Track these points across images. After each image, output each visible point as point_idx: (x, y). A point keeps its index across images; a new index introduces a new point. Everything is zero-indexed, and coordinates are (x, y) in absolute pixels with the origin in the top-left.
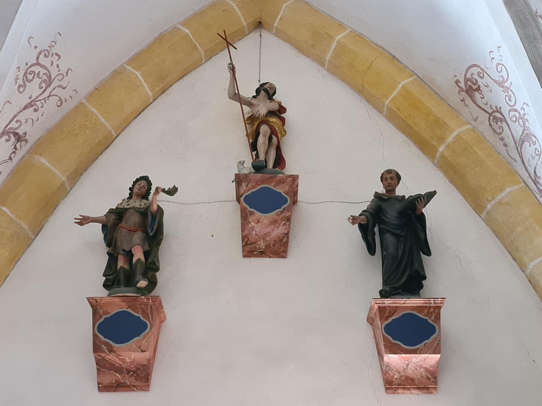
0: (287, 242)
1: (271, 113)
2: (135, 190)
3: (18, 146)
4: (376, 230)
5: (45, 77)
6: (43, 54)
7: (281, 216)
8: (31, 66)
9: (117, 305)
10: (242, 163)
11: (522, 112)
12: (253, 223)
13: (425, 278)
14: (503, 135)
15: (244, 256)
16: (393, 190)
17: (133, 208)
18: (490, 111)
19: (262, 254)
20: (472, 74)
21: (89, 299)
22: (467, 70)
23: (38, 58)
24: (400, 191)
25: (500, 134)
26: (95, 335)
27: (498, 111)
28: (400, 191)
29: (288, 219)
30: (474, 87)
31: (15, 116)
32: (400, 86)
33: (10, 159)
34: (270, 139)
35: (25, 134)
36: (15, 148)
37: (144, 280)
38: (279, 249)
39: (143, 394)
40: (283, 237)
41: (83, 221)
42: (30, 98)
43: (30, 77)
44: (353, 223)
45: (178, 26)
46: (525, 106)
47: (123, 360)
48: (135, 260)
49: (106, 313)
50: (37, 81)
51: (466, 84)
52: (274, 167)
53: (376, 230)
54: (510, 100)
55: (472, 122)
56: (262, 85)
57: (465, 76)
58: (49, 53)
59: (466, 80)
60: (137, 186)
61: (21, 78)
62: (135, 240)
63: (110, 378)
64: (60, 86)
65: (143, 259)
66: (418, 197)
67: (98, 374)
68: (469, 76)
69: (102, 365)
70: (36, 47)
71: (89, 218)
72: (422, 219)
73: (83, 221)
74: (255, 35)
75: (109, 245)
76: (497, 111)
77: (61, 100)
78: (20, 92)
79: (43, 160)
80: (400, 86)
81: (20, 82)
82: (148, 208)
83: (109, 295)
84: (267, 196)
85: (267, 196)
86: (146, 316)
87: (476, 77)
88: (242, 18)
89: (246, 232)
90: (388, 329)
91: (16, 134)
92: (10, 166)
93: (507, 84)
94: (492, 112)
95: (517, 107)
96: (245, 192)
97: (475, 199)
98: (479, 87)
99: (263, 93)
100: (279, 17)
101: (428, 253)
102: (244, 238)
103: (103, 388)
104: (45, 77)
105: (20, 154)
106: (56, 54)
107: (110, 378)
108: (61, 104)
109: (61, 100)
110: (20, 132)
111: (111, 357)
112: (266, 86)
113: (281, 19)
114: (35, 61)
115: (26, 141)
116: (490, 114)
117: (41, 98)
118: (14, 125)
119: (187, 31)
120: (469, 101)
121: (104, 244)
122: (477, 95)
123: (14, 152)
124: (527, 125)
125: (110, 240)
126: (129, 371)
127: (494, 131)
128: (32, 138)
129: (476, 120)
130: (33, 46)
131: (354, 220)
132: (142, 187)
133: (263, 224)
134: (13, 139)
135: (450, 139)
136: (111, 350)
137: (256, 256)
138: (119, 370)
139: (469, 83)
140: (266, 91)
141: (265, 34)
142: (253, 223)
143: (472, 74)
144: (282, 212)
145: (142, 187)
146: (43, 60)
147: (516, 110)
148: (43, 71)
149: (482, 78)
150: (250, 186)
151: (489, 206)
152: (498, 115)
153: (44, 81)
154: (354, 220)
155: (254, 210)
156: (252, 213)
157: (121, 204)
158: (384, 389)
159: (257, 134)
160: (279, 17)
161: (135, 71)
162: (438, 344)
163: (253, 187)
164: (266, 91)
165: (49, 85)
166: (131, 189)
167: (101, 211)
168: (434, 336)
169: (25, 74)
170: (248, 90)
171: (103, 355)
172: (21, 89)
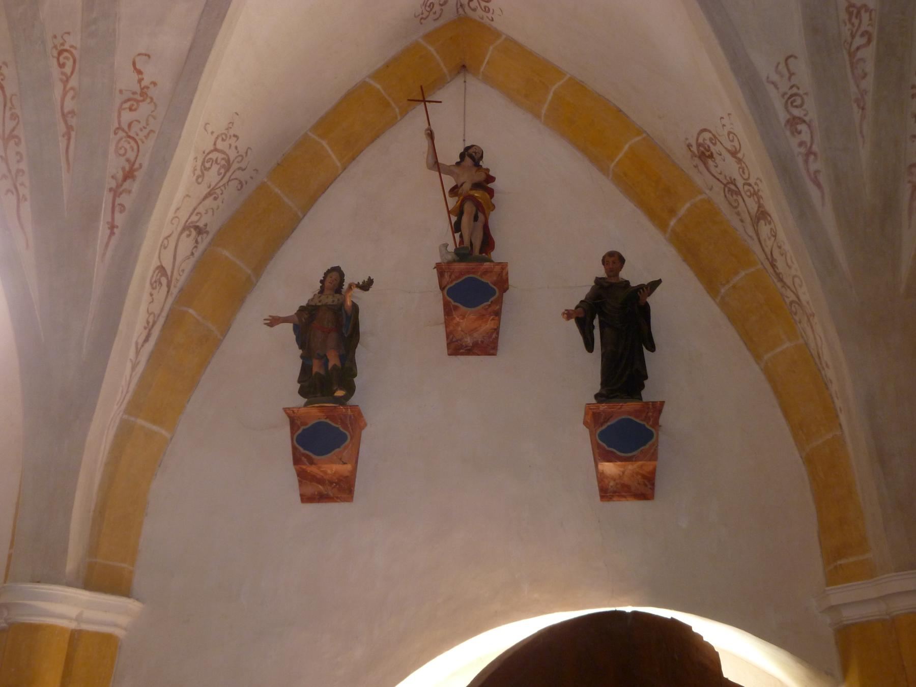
0: (497, 338)
1: (477, 186)
2: (327, 284)
3: (199, 239)
4: (596, 322)
5: (223, 162)
6: (220, 139)
7: (490, 310)
8: (208, 154)
9: (315, 414)
10: (446, 246)
11: (756, 187)
12: (458, 319)
13: (646, 377)
14: (739, 209)
15: (449, 355)
16: (617, 275)
17: (326, 305)
18: (725, 182)
19: (469, 351)
20: (704, 139)
21: (285, 410)
22: (699, 134)
23: (215, 144)
24: (624, 274)
25: (736, 207)
26: (294, 449)
27: (733, 182)
28: (624, 274)
29: (498, 314)
30: (708, 154)
31: (195, 209)
32: (626, 147)
33: (192, 254)
34: (476, 218)
35: (206, 225)
36: (197, 242)
37: (341, 389)
38: (487, 346)
39: (345, 505)
40: (492, 333)
41: (273, 321)
42: (209, 187)
43: (208, 165)
44: (568, 318)
45: (367, 80)
46: (758, 182)
47: (325, 473)
48: (330, 365)
49: (303, 424)
50: (215, 168)
51: (698, 150)
52: (481, 252)
53: (596, 322)
54: (744, 173)
55: (707, 191)
56: (467, 149)
57: (697, 140)
58: (226, 135)
59: (699, 145)
60: (328, 279)
61: (198, 168)
62: (329, 333)
63: (311, 489)
64: (239, 169)
65: (338, 363)
66: (641, 287)
67: (300, 486)
68: (701, 141)
69: (303, 477)
70: (212, 133)
71: (280, 318)
72: (645, 310)
73: (273, 321)
74: (458, 82)
75: (301, 347)
76: (732, 183)
77: (241, 183)
78: (199, 183)
79: (226, 253)
80: (626, 147)
81: (198, 172)
82: (342, 305)
83: (306, 405)
84: (473, 287)
85: (473, 287)
86: (345, 427)
87: (708, 142)
88: (442, 64)
89: (451, 328)
90: (602, 435)
91: (196, 228)
92: (193, 260)
93: (740, 155)
94: (728, 183)
95: (752, 181)
96: (448, 283)
97: (710, 279)
98: (712, 154)
99: (468, 161)
100: (486, 60)
101: (652, 348)
102: (448, 335)
103: (306, 499)
104: (223, 162)
105: (201, 247)
106: (235, 136)
107: (311, 489)
108: (242, 186)
109: (241, 183)
110: (201, 224)
111: (312, 469)
112: (470, 151)
113: (488, 63)
114: (212, 148)
115: (207, 233)
116: (725, 185)
117: (221, 184)
118: (194, 218)
119: (379, 86)
120: (702, 167)
121: (295, 346)
122: (710, 163)
123: (196, 247)
124: (762, 202)
125: (303, 341)
126: (331, 483)
127: (731, 204)
128: (213, 229)
129: (711, 189)
130: (209, 131)
131: (568, 315)
132: (334, 279)
133: (469, 321)
134: (194, 233)
135: (683, 210)
136: (312, 462)
137: (462, 354)
138: (321, 481)
139: (702, 149)
140: (471, 156)
141: (471, 79)
142: (458, 319)
143: (704, 139)
144: (490, 306)
145: (334, 279)
146: (220, 145)
147: (750, 185)
148: (220, 156)
149: (715, 144)
150: (453, 277)
151: (723, 291)
152: (733, 187)
153: (223, 167)
154: (568, 315)
155: (459, 305)
156: (456, 308)
157: (312, 300)
158: (599, 498)
159: (460, 213)
160: (486, 60)
161: (320, 140)
162: (656, 450)
163: (457, 278)
164: (471, 156)
165: (227, 170)
166: (322, 282)
167: (291, 310)
168: (650, 443)
169: (203, 164)
170: (450, 154)
171: (304, 467)
172: (200, 180)
